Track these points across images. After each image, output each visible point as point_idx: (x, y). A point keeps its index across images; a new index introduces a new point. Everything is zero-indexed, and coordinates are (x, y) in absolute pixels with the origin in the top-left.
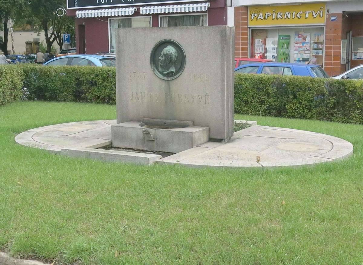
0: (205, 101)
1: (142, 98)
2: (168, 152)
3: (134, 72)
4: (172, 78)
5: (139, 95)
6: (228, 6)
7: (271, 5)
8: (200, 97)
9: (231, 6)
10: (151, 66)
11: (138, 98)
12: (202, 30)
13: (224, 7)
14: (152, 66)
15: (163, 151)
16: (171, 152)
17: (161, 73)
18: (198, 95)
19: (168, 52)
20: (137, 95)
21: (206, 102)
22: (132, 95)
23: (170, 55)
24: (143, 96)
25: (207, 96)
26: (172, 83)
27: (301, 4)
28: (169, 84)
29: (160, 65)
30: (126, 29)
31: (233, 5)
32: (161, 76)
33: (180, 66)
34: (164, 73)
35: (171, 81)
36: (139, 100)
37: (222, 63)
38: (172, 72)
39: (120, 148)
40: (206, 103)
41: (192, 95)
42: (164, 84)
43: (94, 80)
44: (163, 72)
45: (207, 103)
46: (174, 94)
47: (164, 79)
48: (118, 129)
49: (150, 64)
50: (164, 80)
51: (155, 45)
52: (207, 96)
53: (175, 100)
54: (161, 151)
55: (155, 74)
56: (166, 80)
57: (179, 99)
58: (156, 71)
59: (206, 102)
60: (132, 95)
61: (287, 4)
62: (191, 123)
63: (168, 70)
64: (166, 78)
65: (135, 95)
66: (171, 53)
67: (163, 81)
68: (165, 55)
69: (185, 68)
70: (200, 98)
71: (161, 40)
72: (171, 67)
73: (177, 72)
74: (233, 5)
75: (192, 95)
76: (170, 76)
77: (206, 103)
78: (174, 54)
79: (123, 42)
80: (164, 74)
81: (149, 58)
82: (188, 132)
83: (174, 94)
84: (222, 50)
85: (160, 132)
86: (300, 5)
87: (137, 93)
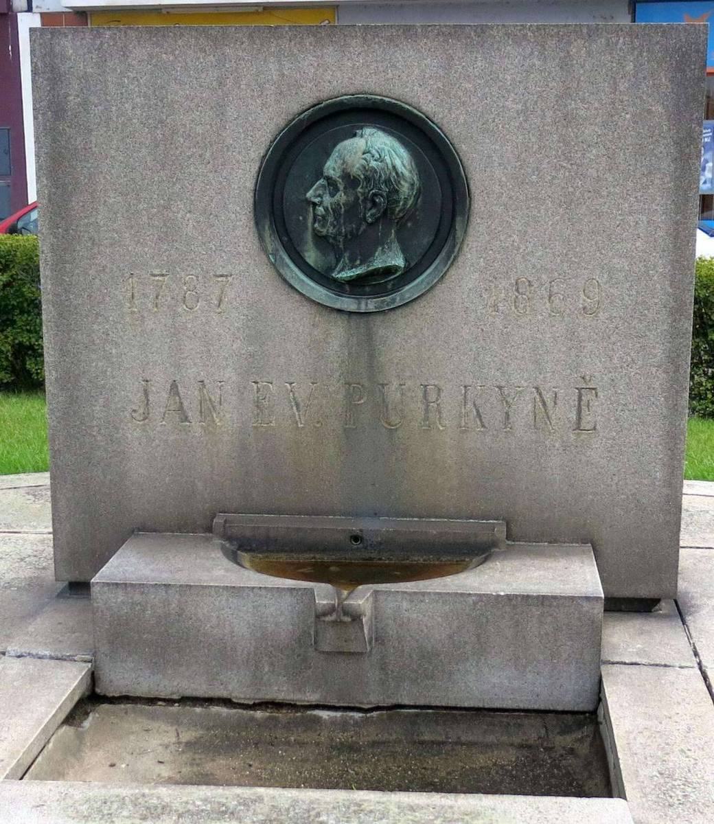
0: (573, 416)
1: (207, 409)
2: (452, 703)
3: (156, 272)
4: (388, 299)
5: (191, 396)
6: (20, 10)
7: (164, 11)
8: (548, 397)
9: (30, 9)
10: (261, 238)
11: (181, 408)
12: (569, 43)
13: (6, 12)
14: (268, 239)
15: (422, 702)
16: (466, 705)
17: (322, 277)
18: (537, 388)
19: (373, 164)
20: (178, 394)
21: (579, 418)
22: (146, 393)
23: (388, 182)
24: (215, 398)
25: (584, 392)
26: (382, 328)
27: (260, 10)
28: (369, 337)
29: (309, 236)
30: (99, 35)
31: (37, 7)
32: (319, 293)
33: (431, 238)
34: (335, 275)
35: (379, 318)
36: (186, 419)
37: (676, 223)
38: (388, 271)
39: (152, 701)
40: (578, 426)
41: (500, 388)
42: (338, 331)
43: (17, 342)
44: (332, 269)
45: (584, 425)
46: (395, 384)
47: (338, 306)
48: (138, 597)
49: (254, 229)
50: (339, 311)
51: (282, 123)
52: (584, 392)
53: (403, 417)
54: (406, 702)
55: (285, 281)
56: (351, 313)
57: (427, 410)
58: (288, 266)
59: (579, 418)
60: (146, 393)
61: (258, 3)
62: (500, 532)
63: (366, 258)
64: (348, 304)
65: (160, 396)
66: (394, 167)
67: (334, 315)
68: (351, 181)
69: (465, 249)
70: (550, 403)
71: (324, 95)
72: (380, 242)
73: (410, 273)
74: (37, 7)
75: (500, 388)
76: (367, 289)
77: (578, 426)
78: (407, 173)
79: (85, 103)
80: (335, 280)
81: (249, 197)
82: (572, 598)
83: (395, 384)
84: (681, 152)
85: (405, 605)
86: (257, 13)
87: (174, 386)
